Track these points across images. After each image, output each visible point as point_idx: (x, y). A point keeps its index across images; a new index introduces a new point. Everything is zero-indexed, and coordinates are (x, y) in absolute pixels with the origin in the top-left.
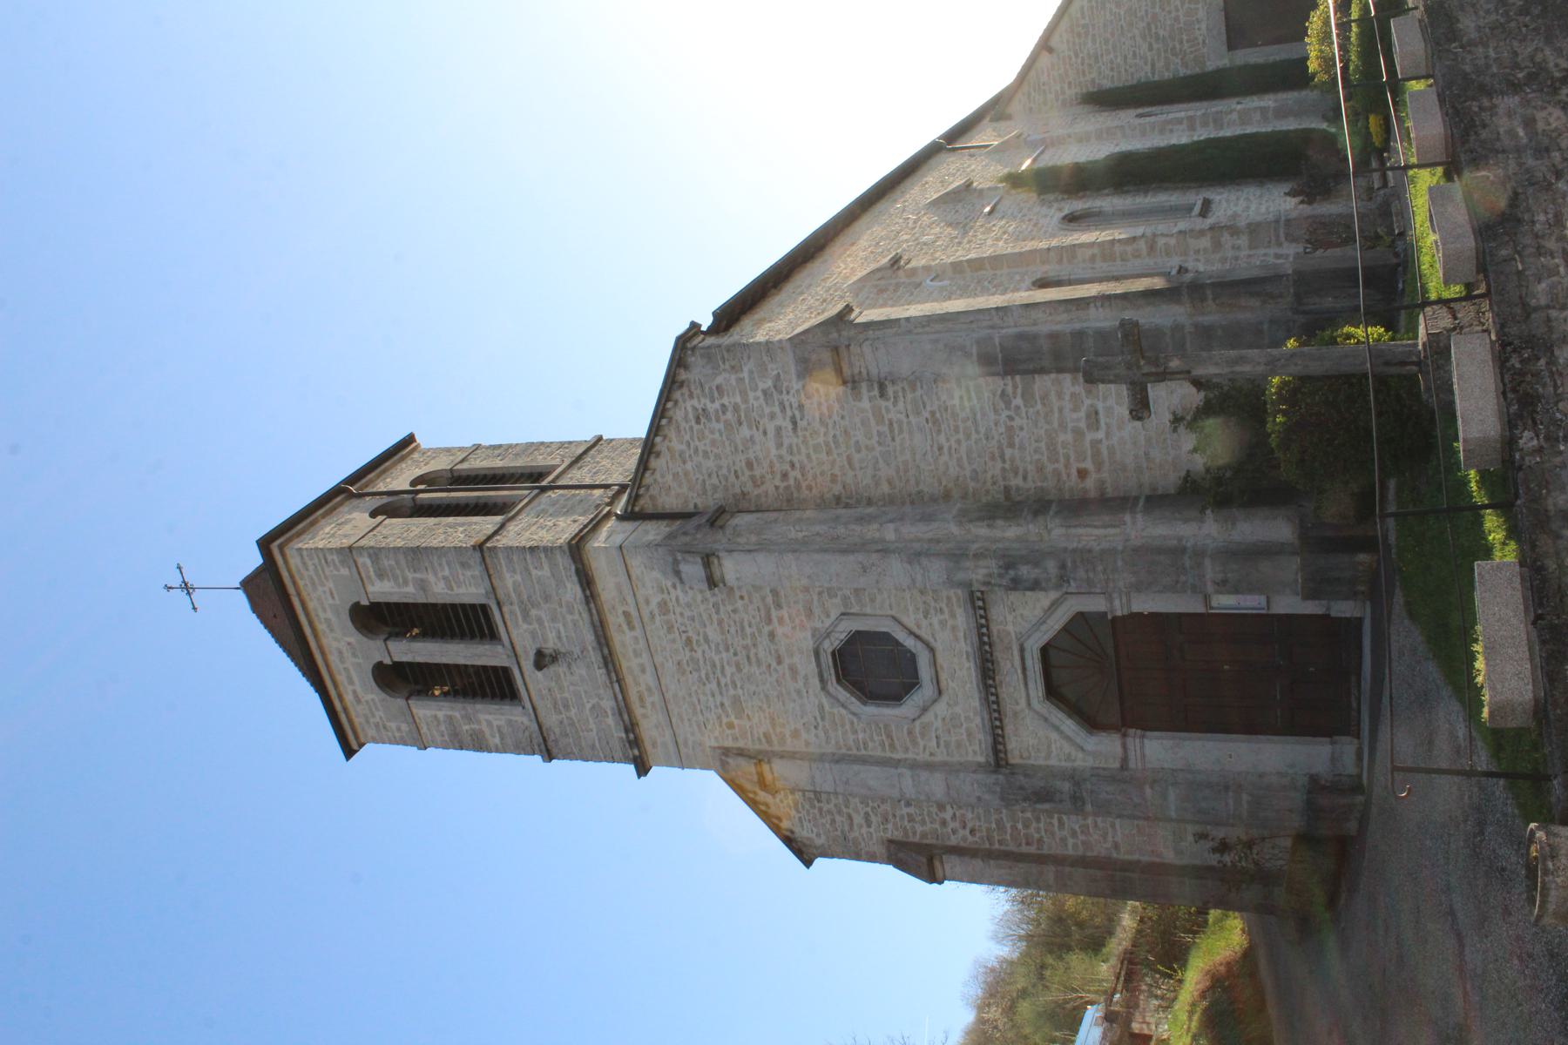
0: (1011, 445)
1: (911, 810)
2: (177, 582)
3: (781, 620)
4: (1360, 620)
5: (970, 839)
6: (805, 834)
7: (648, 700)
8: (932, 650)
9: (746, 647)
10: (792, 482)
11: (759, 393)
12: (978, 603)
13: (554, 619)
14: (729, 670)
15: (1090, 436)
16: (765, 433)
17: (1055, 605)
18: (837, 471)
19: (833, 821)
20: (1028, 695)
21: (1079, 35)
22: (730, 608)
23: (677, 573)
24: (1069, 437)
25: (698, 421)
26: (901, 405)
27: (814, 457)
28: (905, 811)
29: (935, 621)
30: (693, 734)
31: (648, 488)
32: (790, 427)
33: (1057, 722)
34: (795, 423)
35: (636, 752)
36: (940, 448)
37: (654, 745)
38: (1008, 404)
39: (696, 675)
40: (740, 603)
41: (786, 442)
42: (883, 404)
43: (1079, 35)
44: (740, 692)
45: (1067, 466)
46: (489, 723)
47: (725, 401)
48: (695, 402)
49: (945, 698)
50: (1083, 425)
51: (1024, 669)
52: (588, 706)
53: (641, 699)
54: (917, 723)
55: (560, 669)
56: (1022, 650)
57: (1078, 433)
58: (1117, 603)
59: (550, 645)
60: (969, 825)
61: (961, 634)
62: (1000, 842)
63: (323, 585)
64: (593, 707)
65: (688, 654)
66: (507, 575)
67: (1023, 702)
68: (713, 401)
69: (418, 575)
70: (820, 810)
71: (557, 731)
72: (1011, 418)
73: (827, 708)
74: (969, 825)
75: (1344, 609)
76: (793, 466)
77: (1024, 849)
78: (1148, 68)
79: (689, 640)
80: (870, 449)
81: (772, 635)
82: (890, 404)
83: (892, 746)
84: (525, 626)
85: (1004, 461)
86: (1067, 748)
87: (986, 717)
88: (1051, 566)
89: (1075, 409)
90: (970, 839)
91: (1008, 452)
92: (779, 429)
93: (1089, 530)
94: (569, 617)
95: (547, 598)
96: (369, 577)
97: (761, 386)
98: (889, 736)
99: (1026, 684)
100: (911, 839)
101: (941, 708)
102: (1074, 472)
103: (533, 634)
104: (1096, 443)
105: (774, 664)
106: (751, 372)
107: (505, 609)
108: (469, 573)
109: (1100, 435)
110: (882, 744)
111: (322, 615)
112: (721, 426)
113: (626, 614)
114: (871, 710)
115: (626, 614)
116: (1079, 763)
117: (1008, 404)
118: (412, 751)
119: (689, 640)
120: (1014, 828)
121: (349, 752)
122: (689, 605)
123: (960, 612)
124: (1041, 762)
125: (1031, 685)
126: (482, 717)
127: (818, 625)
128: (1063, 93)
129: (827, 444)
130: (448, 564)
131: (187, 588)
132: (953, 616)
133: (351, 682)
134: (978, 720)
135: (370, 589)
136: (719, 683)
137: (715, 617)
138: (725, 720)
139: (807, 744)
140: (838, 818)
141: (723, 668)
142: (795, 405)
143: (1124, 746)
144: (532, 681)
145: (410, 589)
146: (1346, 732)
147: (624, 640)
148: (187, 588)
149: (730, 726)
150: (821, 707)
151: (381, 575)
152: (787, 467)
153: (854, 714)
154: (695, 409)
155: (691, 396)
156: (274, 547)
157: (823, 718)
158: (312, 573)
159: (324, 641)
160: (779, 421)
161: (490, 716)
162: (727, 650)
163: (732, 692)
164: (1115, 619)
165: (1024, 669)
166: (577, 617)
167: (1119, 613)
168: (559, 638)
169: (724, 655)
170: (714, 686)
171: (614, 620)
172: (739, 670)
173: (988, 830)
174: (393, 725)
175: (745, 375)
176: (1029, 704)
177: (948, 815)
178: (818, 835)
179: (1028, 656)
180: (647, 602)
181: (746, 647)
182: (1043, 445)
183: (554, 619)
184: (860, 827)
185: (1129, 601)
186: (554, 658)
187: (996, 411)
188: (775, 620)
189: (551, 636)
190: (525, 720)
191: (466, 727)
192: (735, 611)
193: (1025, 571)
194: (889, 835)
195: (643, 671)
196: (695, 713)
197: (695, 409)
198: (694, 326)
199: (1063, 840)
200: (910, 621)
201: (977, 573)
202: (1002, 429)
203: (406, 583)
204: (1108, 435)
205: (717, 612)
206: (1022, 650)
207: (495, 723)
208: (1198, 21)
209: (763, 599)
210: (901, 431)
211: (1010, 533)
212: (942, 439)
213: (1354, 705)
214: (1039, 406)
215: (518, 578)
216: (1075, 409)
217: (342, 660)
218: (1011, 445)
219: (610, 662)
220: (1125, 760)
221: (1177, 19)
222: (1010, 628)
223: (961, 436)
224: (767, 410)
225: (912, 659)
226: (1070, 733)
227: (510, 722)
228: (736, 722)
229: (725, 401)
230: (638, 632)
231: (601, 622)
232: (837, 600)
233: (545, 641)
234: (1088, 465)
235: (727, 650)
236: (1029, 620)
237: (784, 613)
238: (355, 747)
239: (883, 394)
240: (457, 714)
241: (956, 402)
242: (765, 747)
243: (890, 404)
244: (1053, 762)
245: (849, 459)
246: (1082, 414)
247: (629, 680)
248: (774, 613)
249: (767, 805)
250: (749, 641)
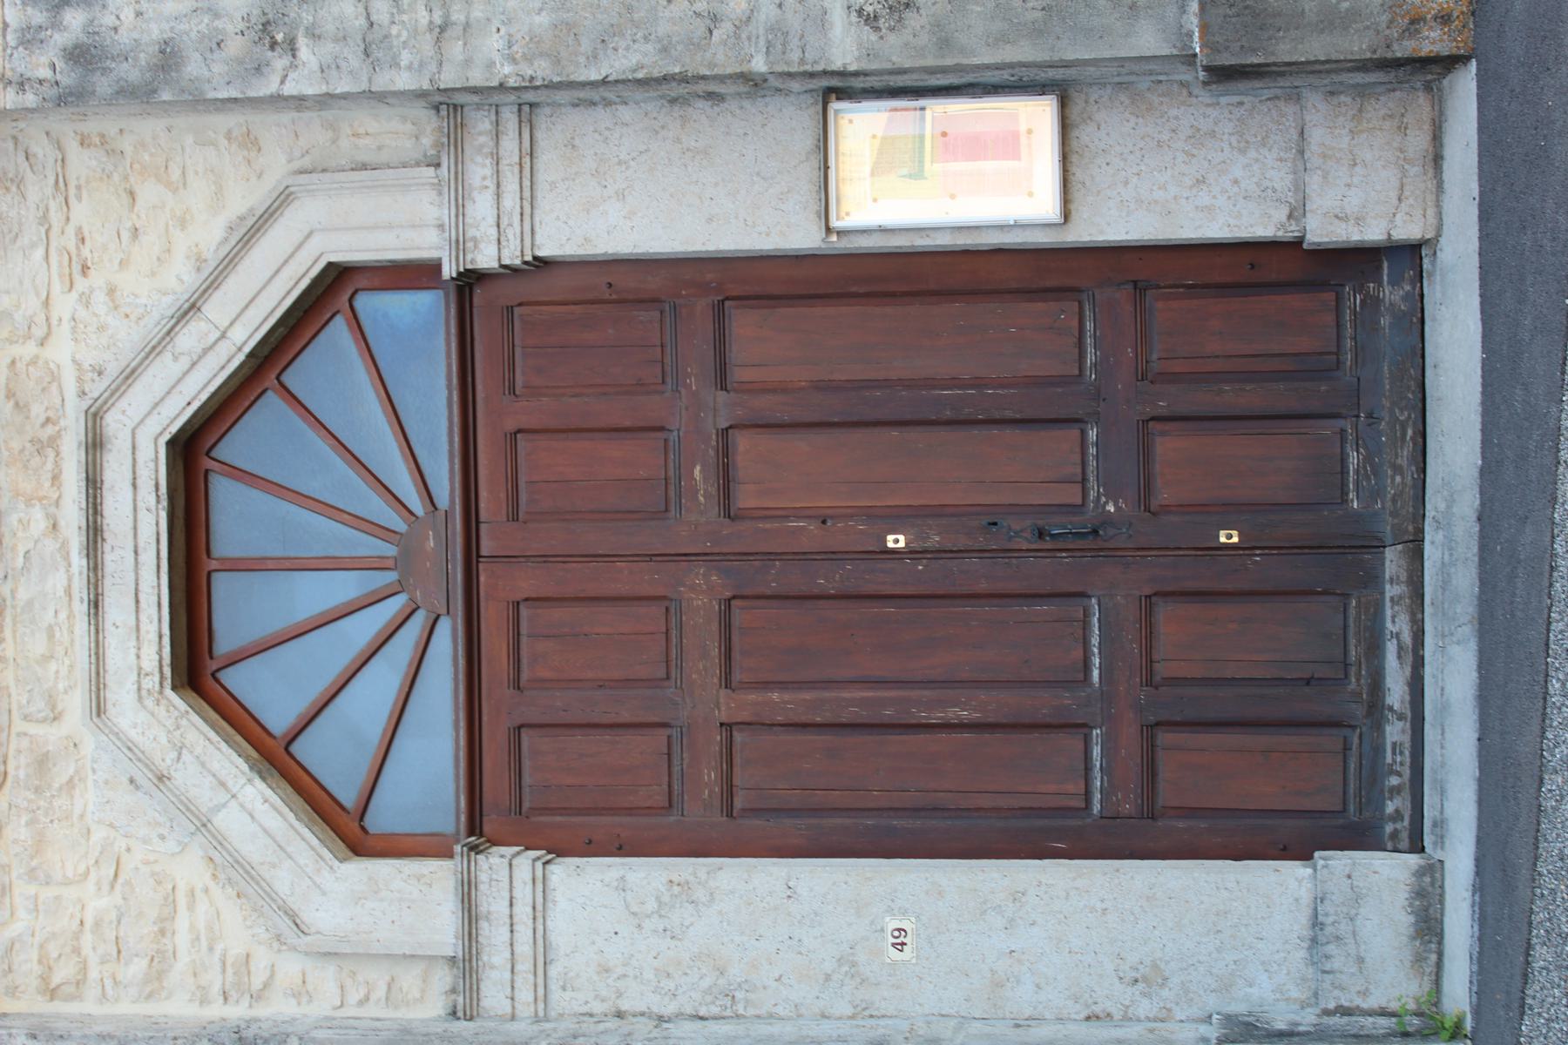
4: (1409, 257)
8: (156, 439)
33: (204, 794)
51: (94, 533)
56: (95, 444)
58: (481, 209)
75: (1353, 183)
86: (239, 931)
116: (278, 1009)
124: (127, 1007)
125: (117, 610)
146: (1360, 835)
152: (620, 971)
165: (94, 533)
167: (485, 258)
179: (115, 471)
185: (529, 199)
206: (95, 444)
213: (1396, 692)
220: (466, 965)
222: (61, 352)
226: (253, 849)
231: (133, 372)
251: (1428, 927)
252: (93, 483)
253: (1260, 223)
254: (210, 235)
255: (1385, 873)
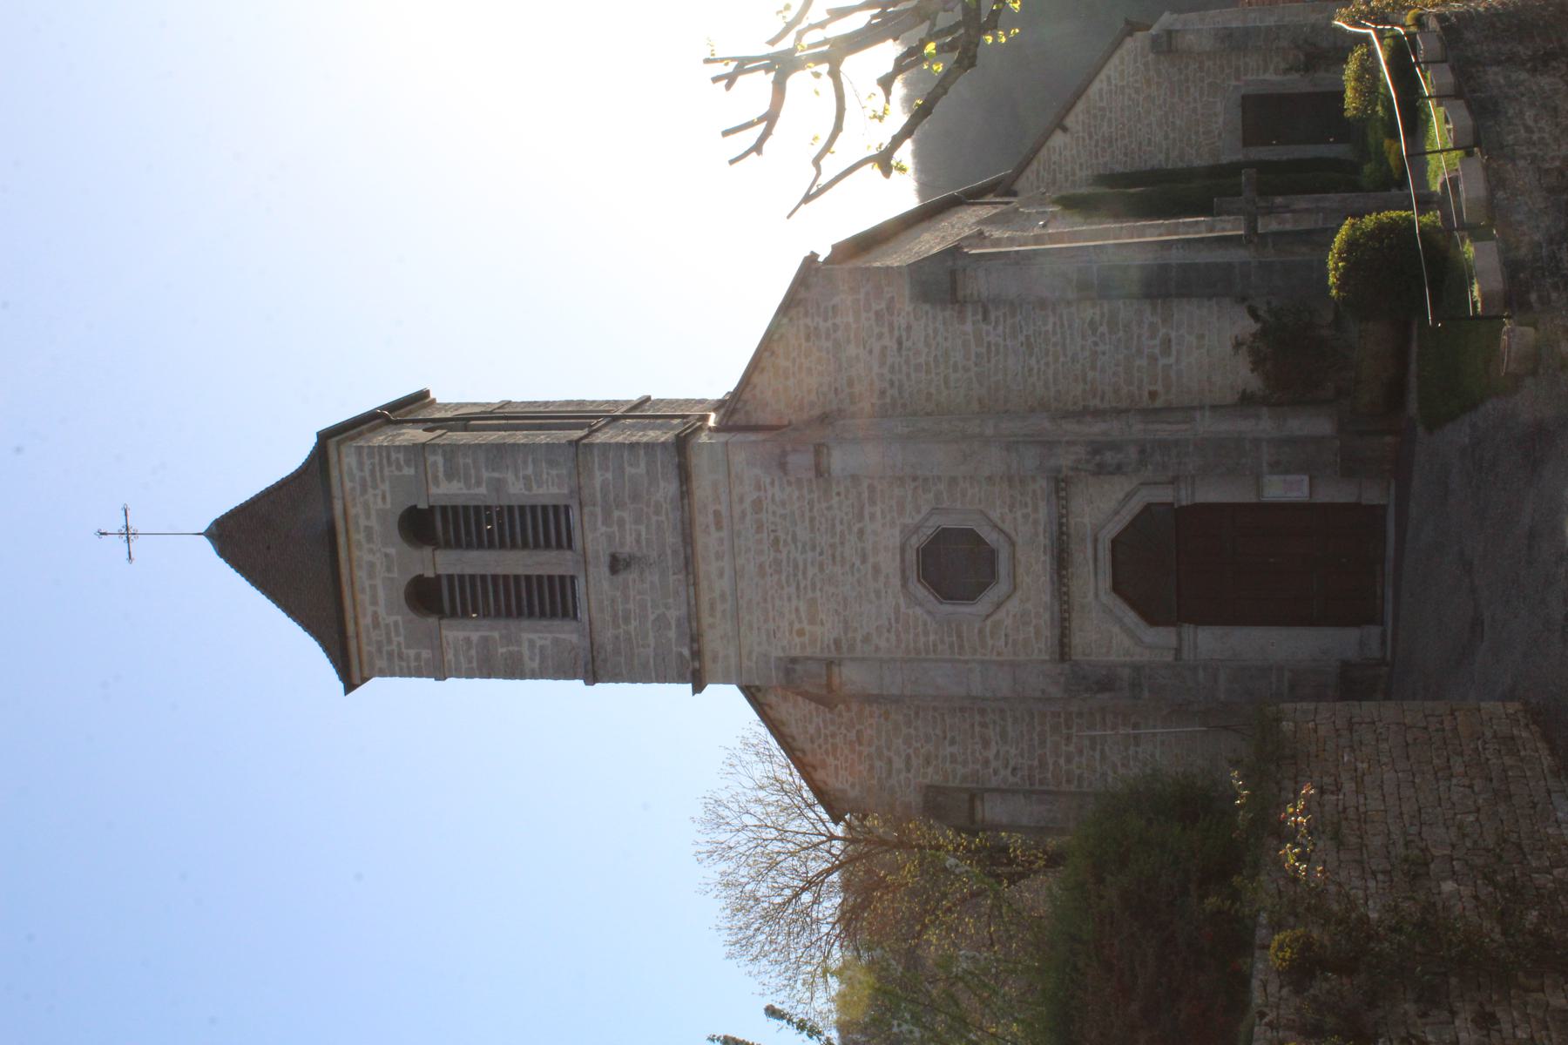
0: (1093, 368)
1: (954, 749)
2: (119, 525)
3: (872, 517)
4: (1384, 507)
5: (1011, 779)
6: (839, 785)
7: (719, 607)
8: (1013, 544)
9: (832, 546)
10: (888, 400)
11: (872, 315)
12: (1061, 485)
13: (637, 521)
14: (811, 571)
15: (1162, 361)
16: (871, 352)
17: (1129, 496)
18: (933, 390)
19: (872, 767)
20: (1097, 588)
21: (1095, 117)
22: (824, 505)
23: (783, 466)
24: (1144, 362)
25: (808, 338)
26: (1001, 328)
27: (913, 376)
28: (949, 750)
29: (1019, 514)
30: (760, 644)
31: (746, 402)
32: (895, 347)
34: (900, 343)
35: (697, 665)
36: (1031, 370)
37: (715, 659)
38: (1094, 331)
39: (776, 577)
40: (835, 500)
41: (889, 361)
42: (985, 327)
43: (1095, 117)
44: (818, 594)
45: (1139, 388)
46: (532, 643)
47: (838, 320)
48: (808, 321)
49: (1019, 593)
50: (1157, 351)
52: (652, 617)
53: (712, 608)
54: (989, 622)
55: (631, 576)
56: (1096, 541)
57: (1153, 359)
58: (1183, 493)
59: (628, 548)
60: (1012, 763)
61: (1041, 529)
62: (1041, 782)
63: (375, 487)
64: (657, 619)
65: (772, 554)
66: (598, 474)
67: (1091, 595)
68: (826, 320)
69: (496, 475)
70: (860, 754)
71: (609, 648)
72: (1096, 344)
73: (903, 609)
74: (1012, 763)
76: (892, 384)
77: (1065, 787)
78: (1162, 157)
79: (777, 540)
80: (966, 370)
81: (861, 532)
82: (990, 328)
83: (961, 647)
84: (603, 529)
85: (1085, 382)
87: (1056, 608)
88: (1133, 453)
89: (1152, 337)
90: (1011, 779)
91: (1090, 375)
92: (884, 348)
93: (1165, 426)
94: (654, 519)
95: (635, 497)
96: (436, 478)
97: (875, 307)
98: (960, 636)
99: (1096, 574)
100: (951, 784)
101: (1013, 606)
102: (1146, 394)
103: (610, 538)
104: (1167, 367)
105: (858, 563)
106: (867, 294)
107: (586, 510)
108: (554, 472)
109: (1172, 360)
110: (951, 646)
111: (363, 522)
112: (829, 344)
113: (717, 514)
114: (947, 608)
115: (717, 514)
117: (1094, 331)
118: (428, 683)
119: (777, 540)
120: (1055, 763)
121: (350, 687)
122: (783, 504)
123: (1042, 505)
126: (525, 636)
127: (908, 521)
128: (1074, 174)
129: (927, 364)
130: (534, 461)
131: (127, 534)
132: (1036, 510)
133: (374, 602)
134: (1047, 616)
135: (433, 490)
136: (798, 587)
137: (807, 514)
138: (797, 626)
139: (877, 648)
140: (878, 764)
141: (805, 567)
142: (904, 326)
143: (1179, 636)
144: (597, 589)
145: (483, 490)
147: (708, 541)
148: (127, 534)
149: (801, 633)
150: (897, 607)
151: (450, 476)
152: (886, 385)
153: (929, 612)
154: (807, 327)
155: (806, 314)
156: (332, 443)
157: (897, 620)
158: (367, 473)
159: (356, 553)
160: (887, 341)
161: (535, 635)
162: (813, 548)
163: (810, 594)
164: (1182, 507)
165: (1096, 559)
166: (663, 518)
167: (1184, 503)
168: (638, 541)
169: (810, 555)
170: (793, 589)
171: (703, 519)
172: (821, 569)
173: (1031, 768)
174: (412, 653)
175: (862, 296)
176: (1096, 595)
177: (991, 754)
178: (853, 786)
179: (1100, 547)
180: (741, 500)
181: (832, 546)
182: (1121, 369)
183: (637, 521)
184: (899, 772)
186: (628, 565)
187: (1083, 337)
188: (867, 517)
189: (630, 539)
190: (574, 638)
191: (502, 650)
192: (829, 508)
193: (1110, 457)
194: (927, 781)
195: (721, 575)
196: (766, 621)
197: (807, 327)
198: (811, 260)
199: (1104, 774)
200: (995, 515)
201: (1065, 460)
202: (1087, 353)
203: (479, 484)
204: (1178, 360)
205: (811, 510)
206: (1096, 541)
207: (539, 643)
208: (1216, 115)
209: (860, 494)
210: (997, 352)
211: (1096, 429)
212: (1033, 361)
214: (1121, 333)
215: (609, 476)
216: (1152, 337)
217: (371, 576)
218: (1093, 368)
219: (689, 564)
220: (1178, 651)
221: (1195, 110)
222: (1086, 520)
223: (1050, 359)
224: (876, 330)
225: (991, 556)
227: (556, 642)
228: (807, 628)
229: (838, 320)
230: (724, 534)
232: (931, 496)
233: (622, 544)
234: (1159, 387)
235: (813, 548)
236: (1103, 509)
237: (878, 510)
238: (357, 681)
239: (985, 318)
240: (496, 635)
241: (1050, 327)
242: (834, 654)
243: (990, 328)
244: (1113, 658)
245: (946, 381)
246: (1157, 342)
247: (704, 584)
248: (867, 510)
249: (804, 752)
250: (837, 540)
251: (1383, 643)
252: (1095, 549)
253: (1352, 499)
254: (1121, 496)
255: (1375, 631)
